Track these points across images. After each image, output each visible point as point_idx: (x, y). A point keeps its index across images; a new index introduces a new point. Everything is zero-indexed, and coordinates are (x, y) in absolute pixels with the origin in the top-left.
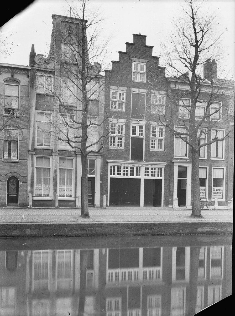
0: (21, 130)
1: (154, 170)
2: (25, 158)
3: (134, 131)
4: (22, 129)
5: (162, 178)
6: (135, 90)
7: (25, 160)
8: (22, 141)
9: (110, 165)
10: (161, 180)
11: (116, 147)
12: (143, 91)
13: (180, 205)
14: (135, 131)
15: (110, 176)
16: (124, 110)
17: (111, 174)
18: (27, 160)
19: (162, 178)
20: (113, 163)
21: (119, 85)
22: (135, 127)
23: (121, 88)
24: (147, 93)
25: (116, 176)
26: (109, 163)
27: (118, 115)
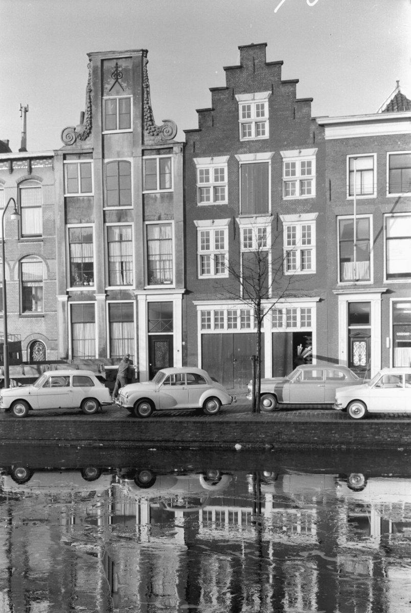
0: (45, 261)
1: (276, 320)
2: (53, 309)
3: (292, 236)
4: (47, 260)
5: (313, 329)
7: (54, 313)
8: (47, 280)
10: (310, 334)
11: (212, 275)
12: (265, 157)
13: (189, 547)
14: (294, 236)
15: (200, 332)
16: (226, 202)
17: (203, 327)
18: (56, 311)
19: (313, 329)
20: (215, 306)
21: (213, 151)
22: (294, 228)
23: (216, 159)
24: (273, 158)
25: (212, 331)
26: (197, 306)
27: (213, 213)
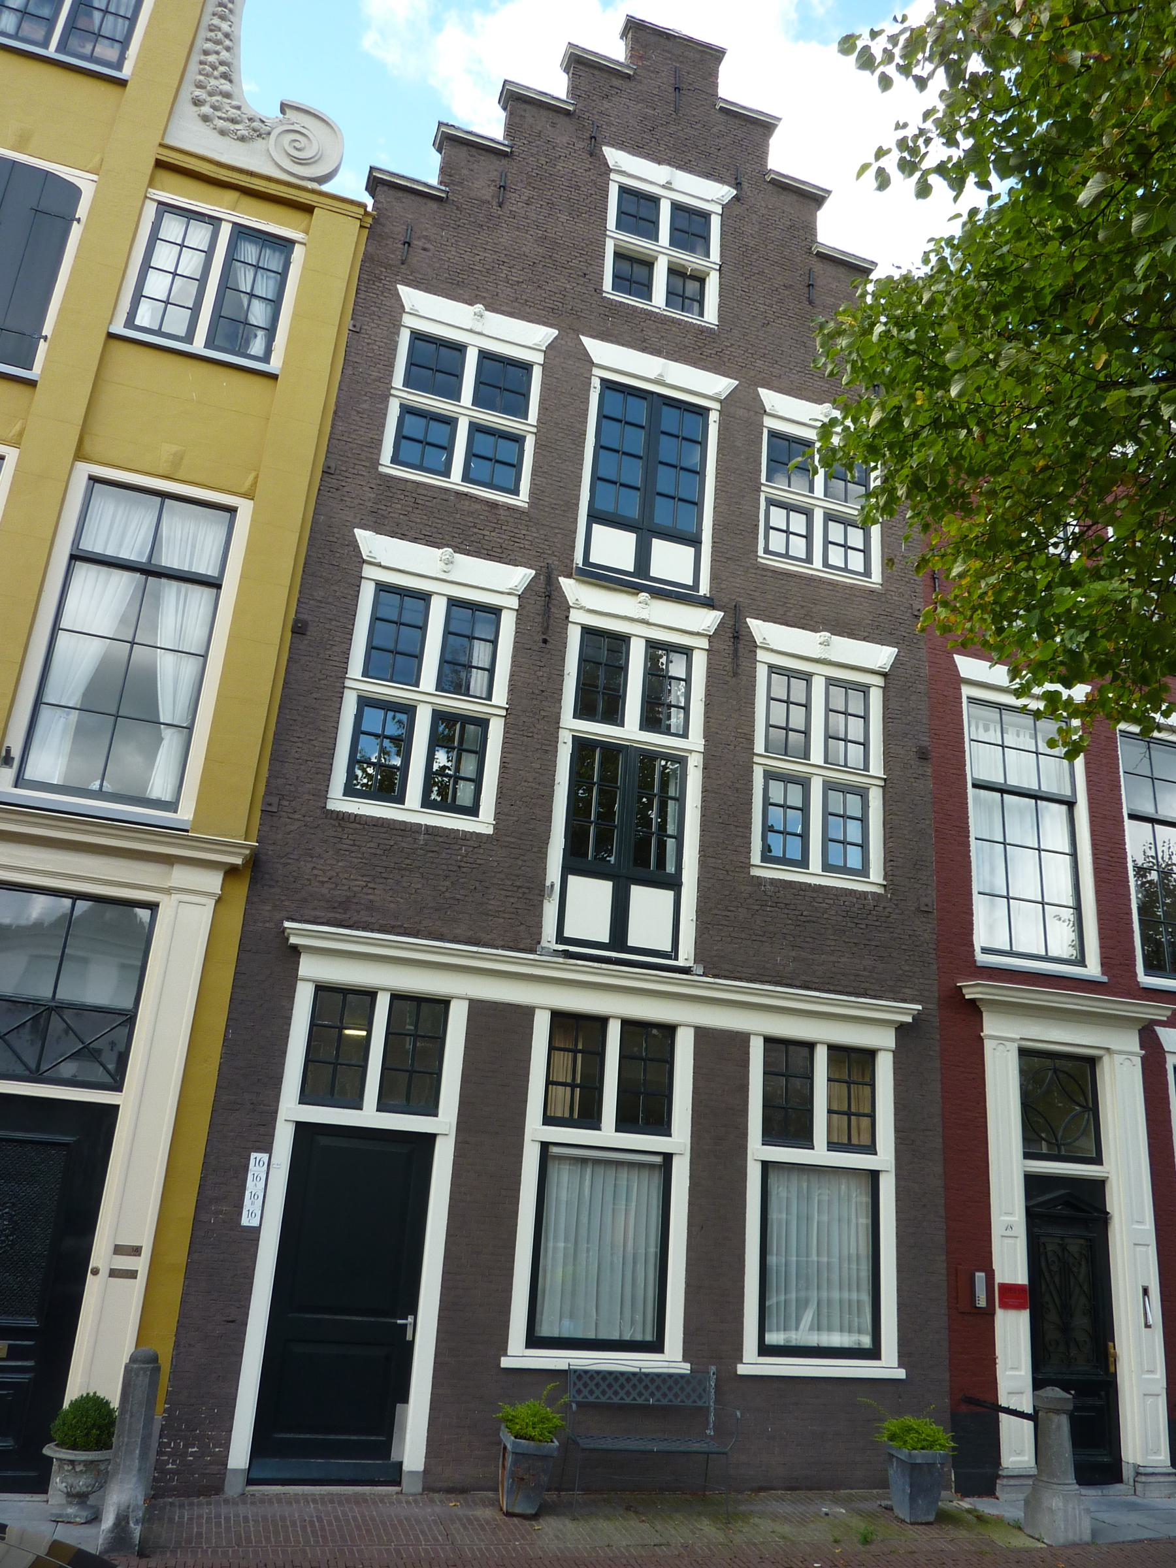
6: (602, 352)
9: (311, 969)
